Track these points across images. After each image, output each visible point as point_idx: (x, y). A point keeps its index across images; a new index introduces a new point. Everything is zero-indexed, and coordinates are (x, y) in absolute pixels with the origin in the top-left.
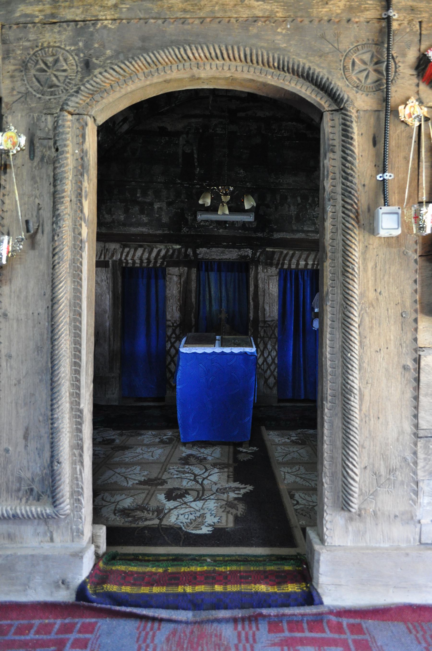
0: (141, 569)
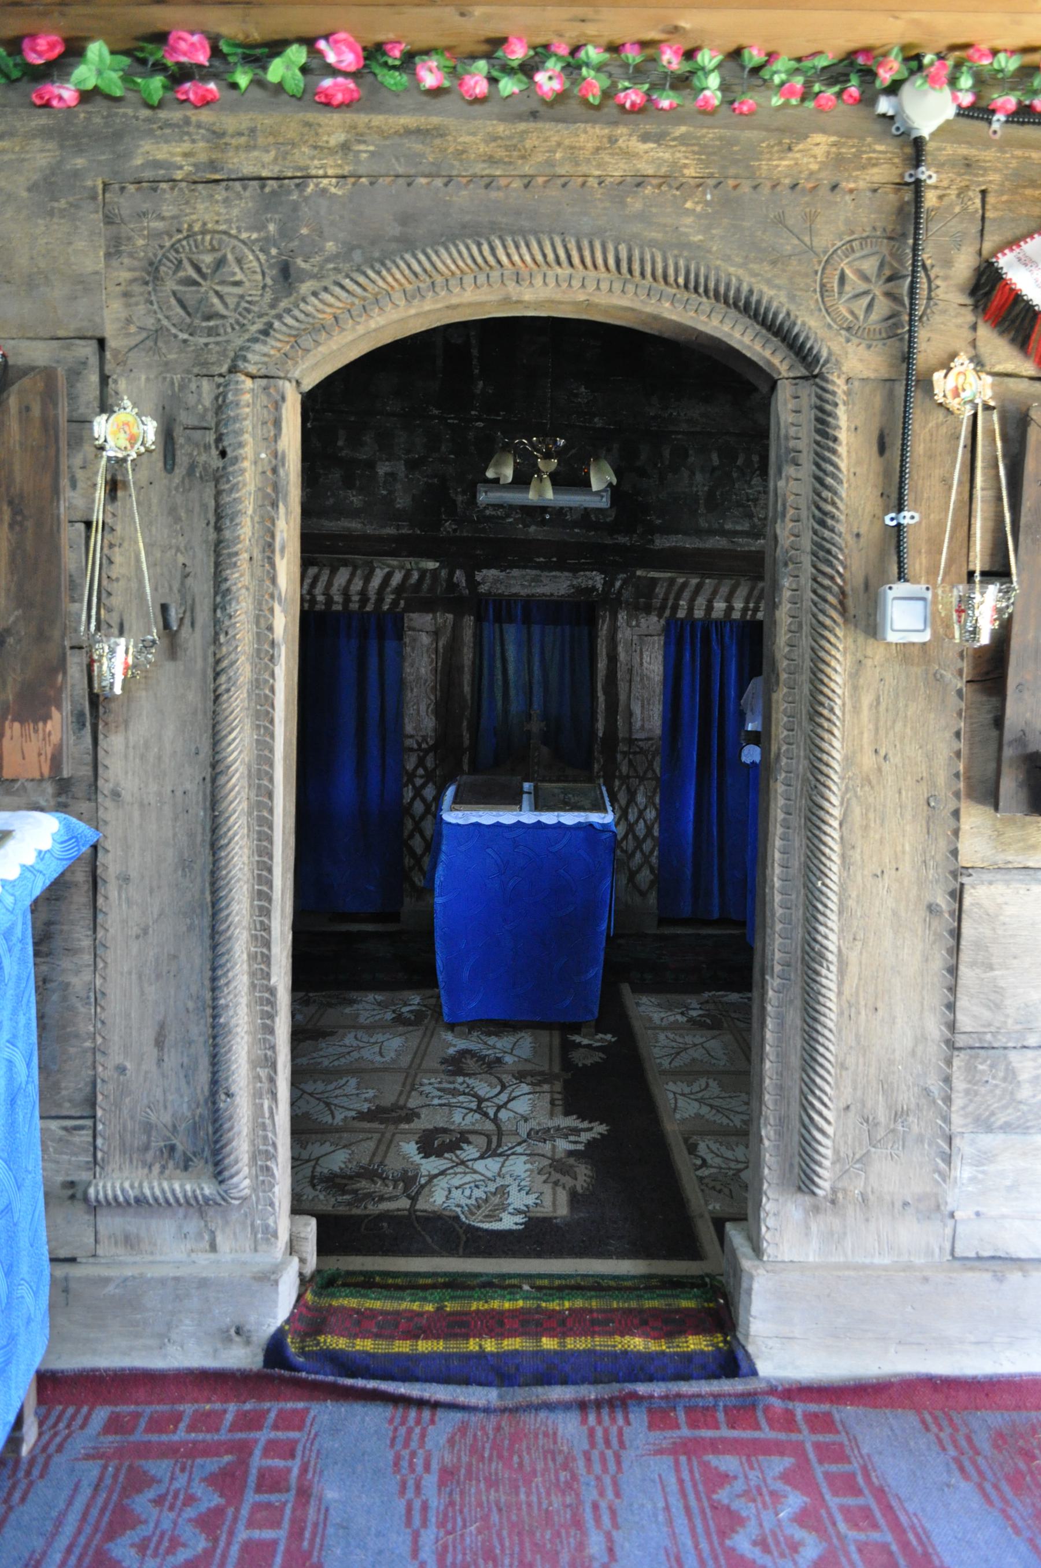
0: (389, 1305)
